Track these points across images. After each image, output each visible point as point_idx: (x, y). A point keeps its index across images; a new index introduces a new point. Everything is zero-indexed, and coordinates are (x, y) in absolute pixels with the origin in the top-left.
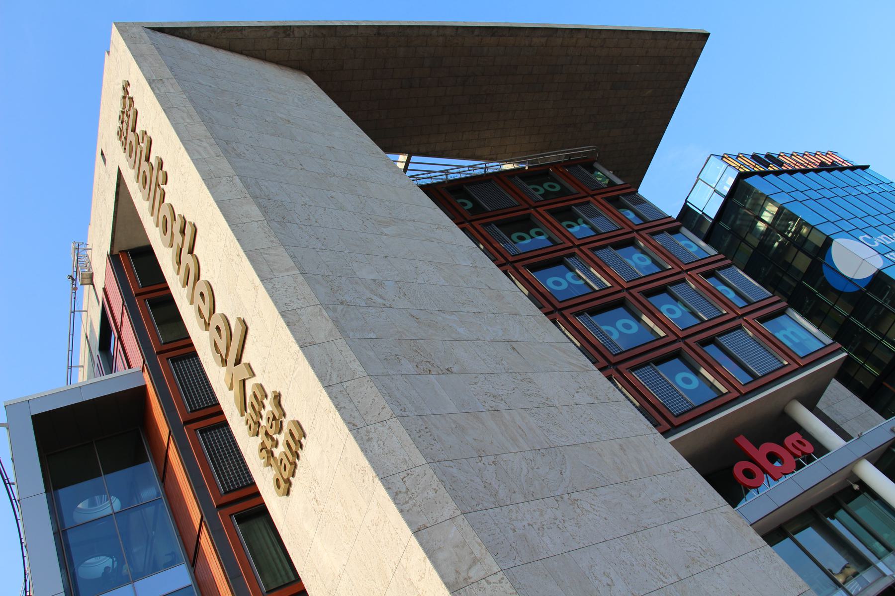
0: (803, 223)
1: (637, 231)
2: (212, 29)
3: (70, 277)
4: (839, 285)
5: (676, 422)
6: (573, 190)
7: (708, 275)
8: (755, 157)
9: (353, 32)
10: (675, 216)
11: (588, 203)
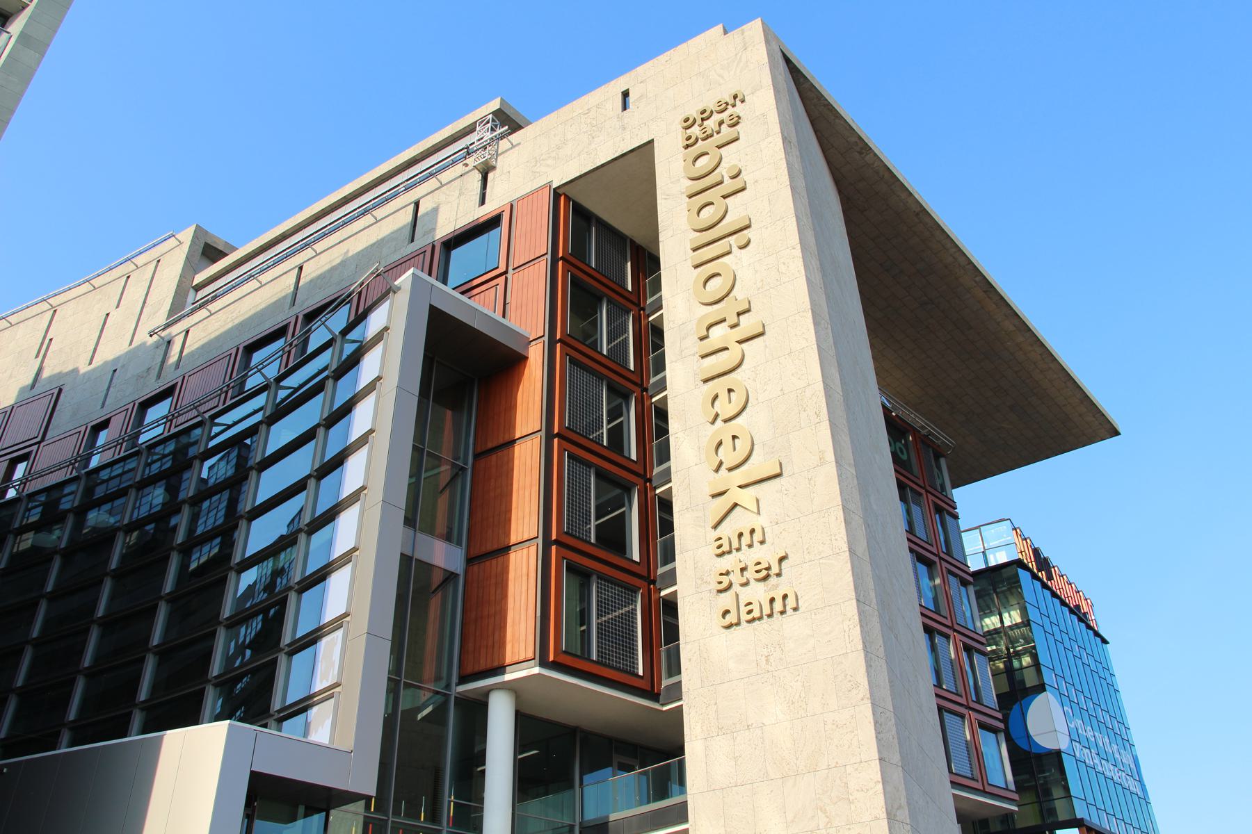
1: (941, 558)
2: (820, 96)
3: (1038, 412)
5: (988, 789)
6: (916, 469)
8: (1036, 552)
9: (903, 196)
10: (972, 569)
11: (920, 494)
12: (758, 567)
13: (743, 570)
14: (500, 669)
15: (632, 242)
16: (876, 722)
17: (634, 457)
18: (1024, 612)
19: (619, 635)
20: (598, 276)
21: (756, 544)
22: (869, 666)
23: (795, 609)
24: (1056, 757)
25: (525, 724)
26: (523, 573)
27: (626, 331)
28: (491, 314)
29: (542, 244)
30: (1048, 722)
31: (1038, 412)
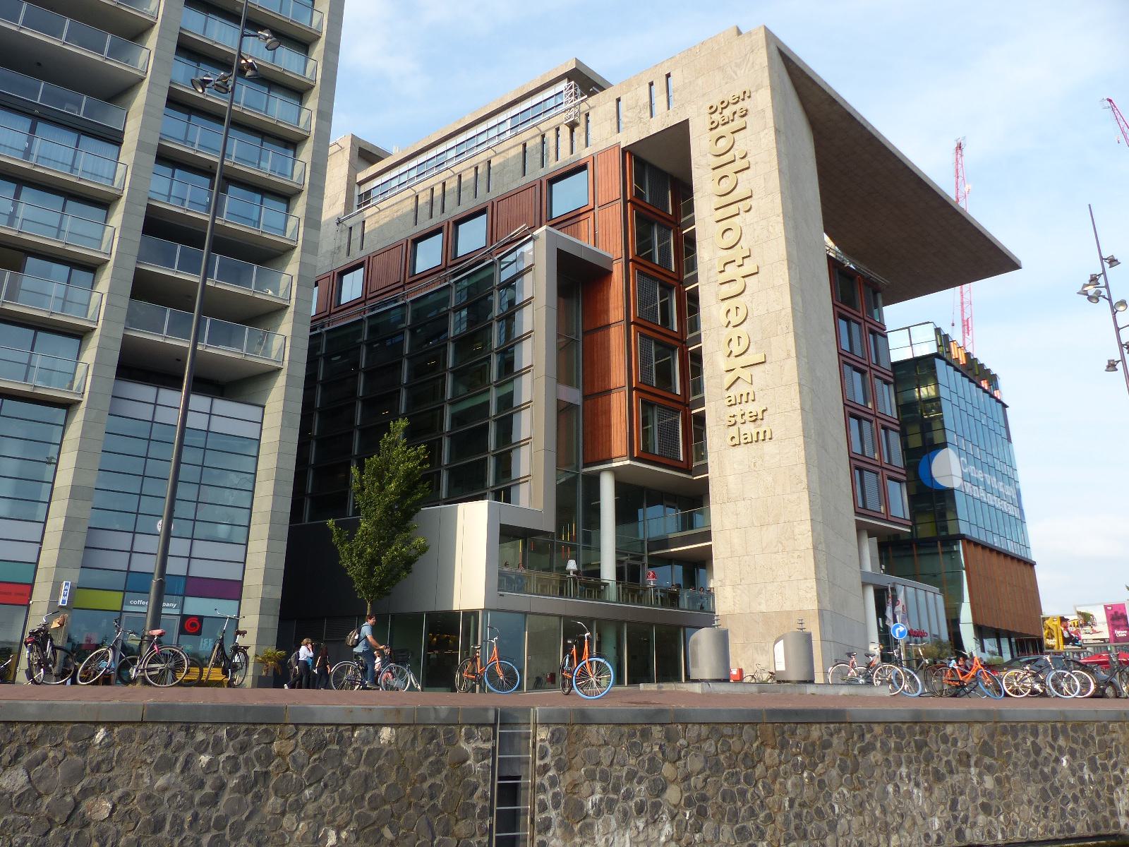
0: (941, 419)
3: (961, 252)
4: (922, 473)
7: (884, 428)
12: (751, 415)
13: (742, 415)
14: (610, 460)
15: (672, 176)
16: (810, 501)
17: (676, 329)
18: (937, 390)
19: (668, 435)
20: (652, 209)
21: (750, 401)
22: (808, 471)
23: (770, 439)
24: (948, 494)
25: (622, 490)
26: (619, 405)
27: (669, 238)
28: (587, 246)
29: (616, 192)
30: (948, 468)
31: (961, 252)
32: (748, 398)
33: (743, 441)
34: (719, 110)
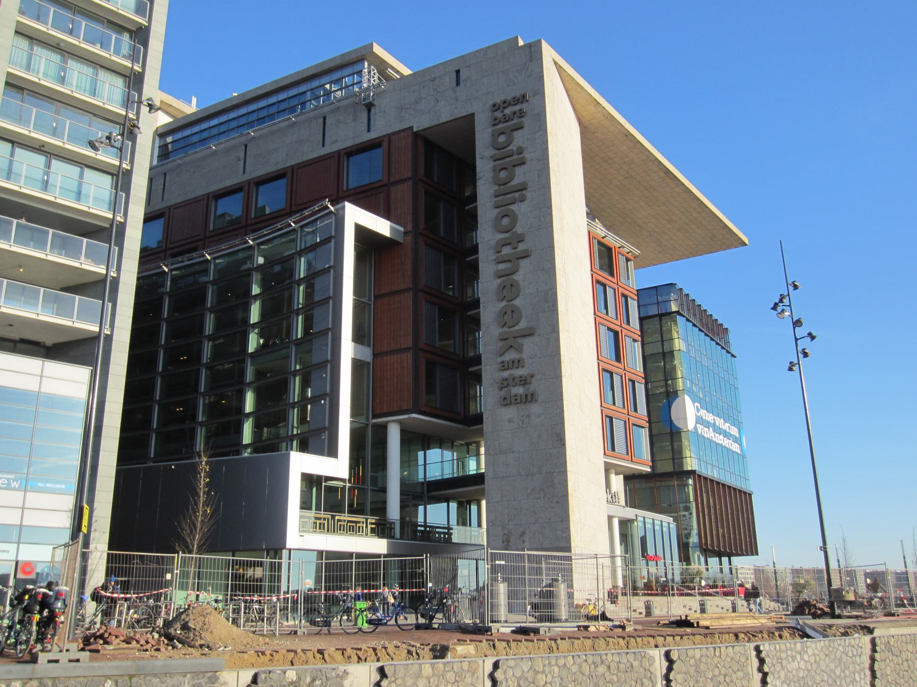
32: (518, 363)
33: (513, 401)
34: (501, 108)
